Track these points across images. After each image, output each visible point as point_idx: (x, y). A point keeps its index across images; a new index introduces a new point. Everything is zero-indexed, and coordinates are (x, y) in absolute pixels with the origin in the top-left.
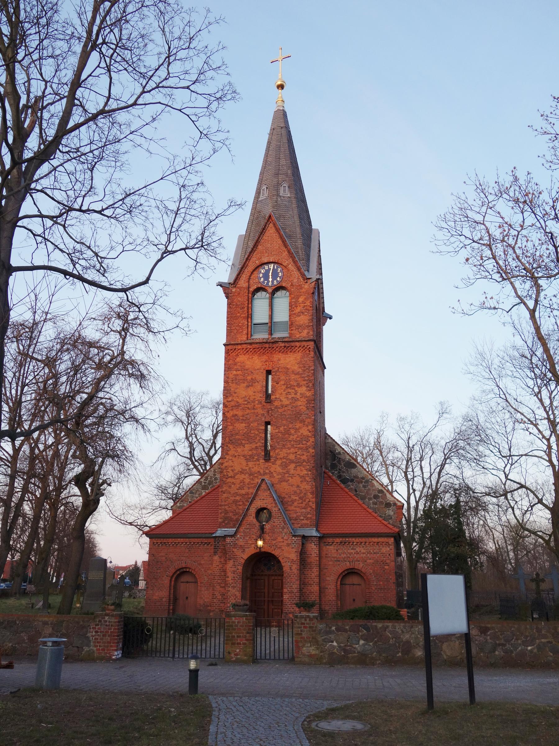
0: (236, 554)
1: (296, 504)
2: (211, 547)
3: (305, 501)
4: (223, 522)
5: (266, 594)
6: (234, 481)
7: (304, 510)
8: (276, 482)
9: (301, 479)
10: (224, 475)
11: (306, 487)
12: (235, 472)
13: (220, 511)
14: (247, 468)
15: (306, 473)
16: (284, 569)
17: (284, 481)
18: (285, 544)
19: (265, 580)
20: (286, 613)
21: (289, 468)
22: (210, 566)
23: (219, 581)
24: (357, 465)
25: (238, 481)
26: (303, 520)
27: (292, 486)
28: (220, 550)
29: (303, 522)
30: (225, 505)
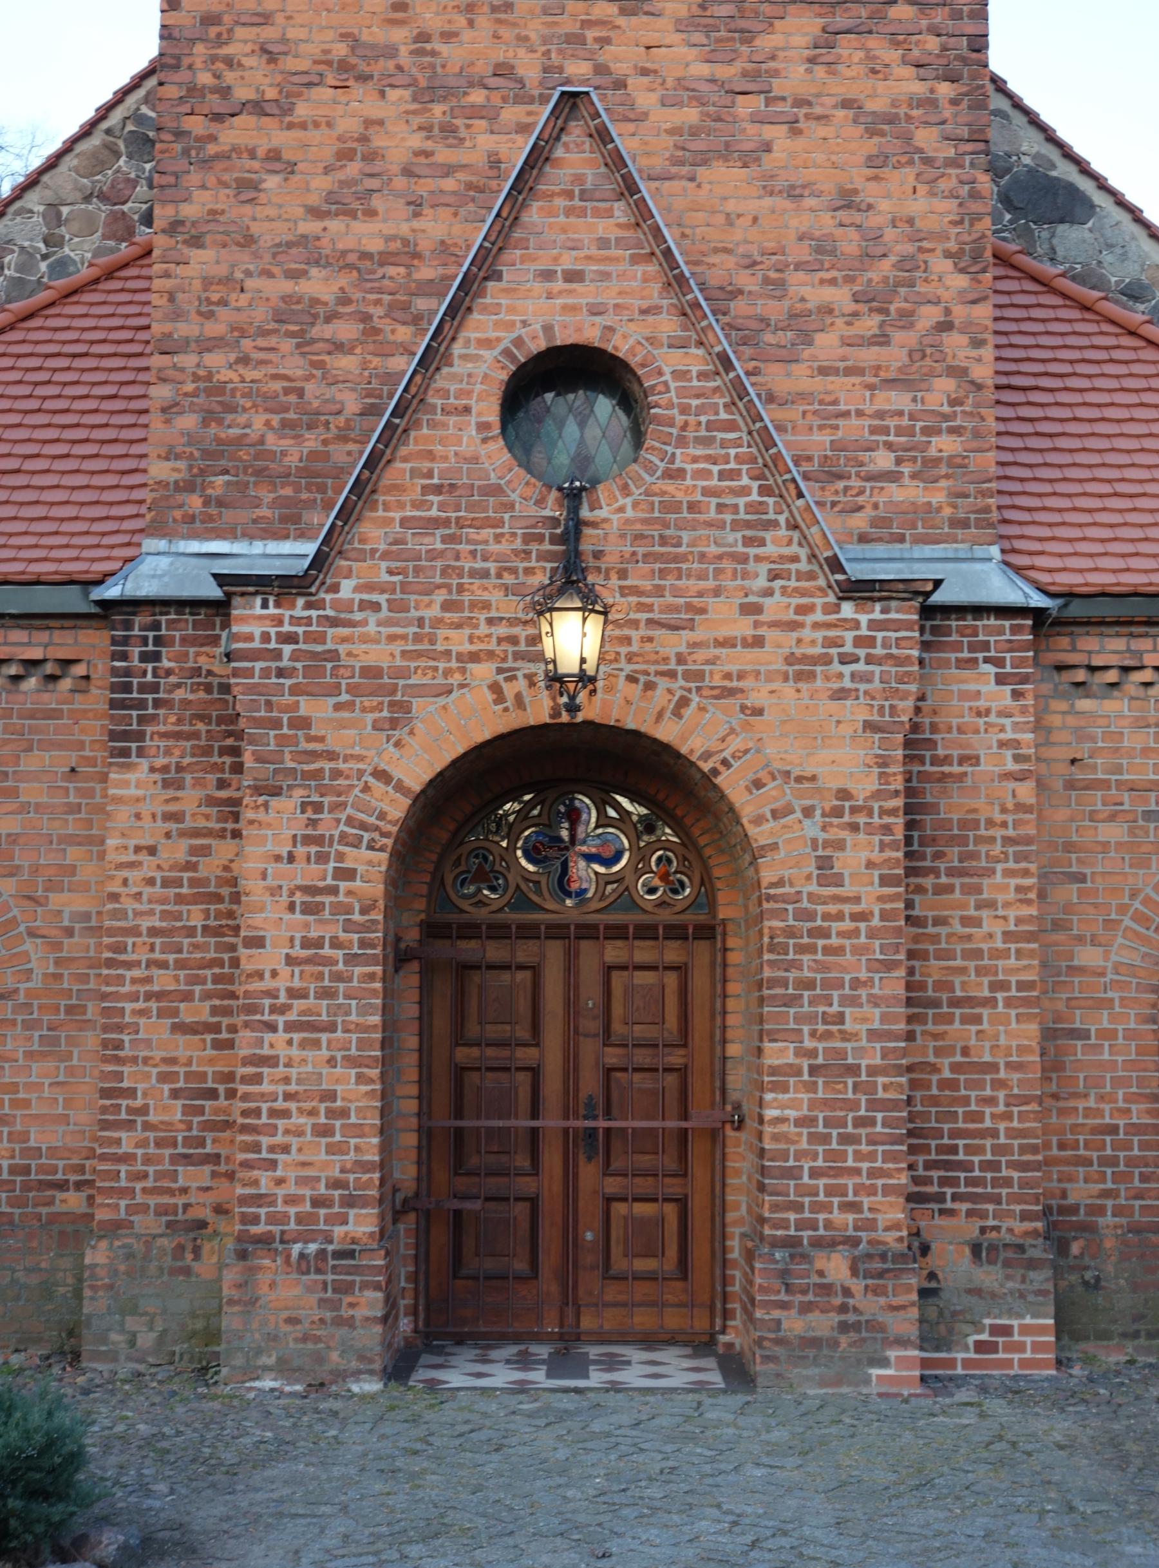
0: (333, 742)
1: (827, 344)
2: (80, 703)
3: (907, 319)
4: (189, 487)
5: (552, 1085)
6: (281, 138)
7: (899, 400)
8: (659, 163)
9: (872, 145)
10: (193, 90)
11: (918, 206)
12: (290, 64)
13: (161, 393)
14: (399, 35)
15: (918, 88)
16: (768, 875)
17: (726, 153)
18: (771, 657)
19: (535, 970)
20: (792, 1243)
21: (766, 42)
22: (73, 854)
23: (163, 980)
24: (1100, 199)
25: (322, 144)
26: (892, 477)
27: (794, 193)
28: (168, 721)
29: (897, 493)
30: (207, 345)
